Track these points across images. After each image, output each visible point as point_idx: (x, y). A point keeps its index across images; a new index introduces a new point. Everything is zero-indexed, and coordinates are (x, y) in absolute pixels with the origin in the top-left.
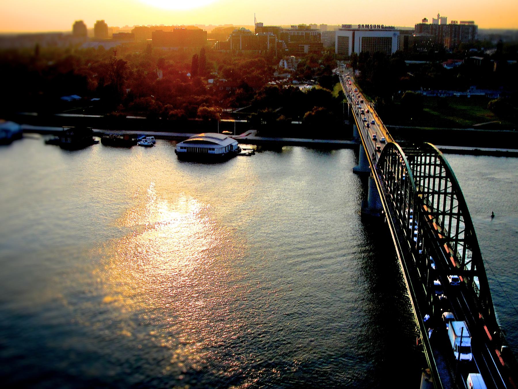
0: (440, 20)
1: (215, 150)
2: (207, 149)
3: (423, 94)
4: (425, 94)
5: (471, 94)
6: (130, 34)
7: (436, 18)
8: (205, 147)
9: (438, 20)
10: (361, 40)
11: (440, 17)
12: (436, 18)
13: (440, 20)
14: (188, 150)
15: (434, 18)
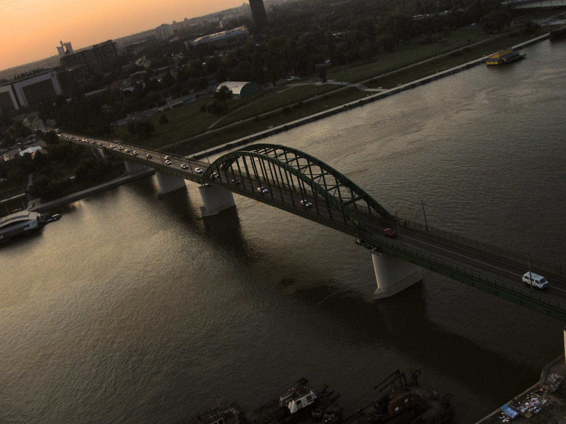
0: (64, 47)
1: (30, 225)
2: (22, 227)
3: (132, 119)
4: (134, 119)
5: (172, 105)
6: (72, 50)
7: (60, 46)
8: (17, 228)
9: (62, 48)
10: (22, 90)
11: (63, 43)
12: (60, 46)
13: (64, 47)
14: (4, 236)
15: (71, 43)
